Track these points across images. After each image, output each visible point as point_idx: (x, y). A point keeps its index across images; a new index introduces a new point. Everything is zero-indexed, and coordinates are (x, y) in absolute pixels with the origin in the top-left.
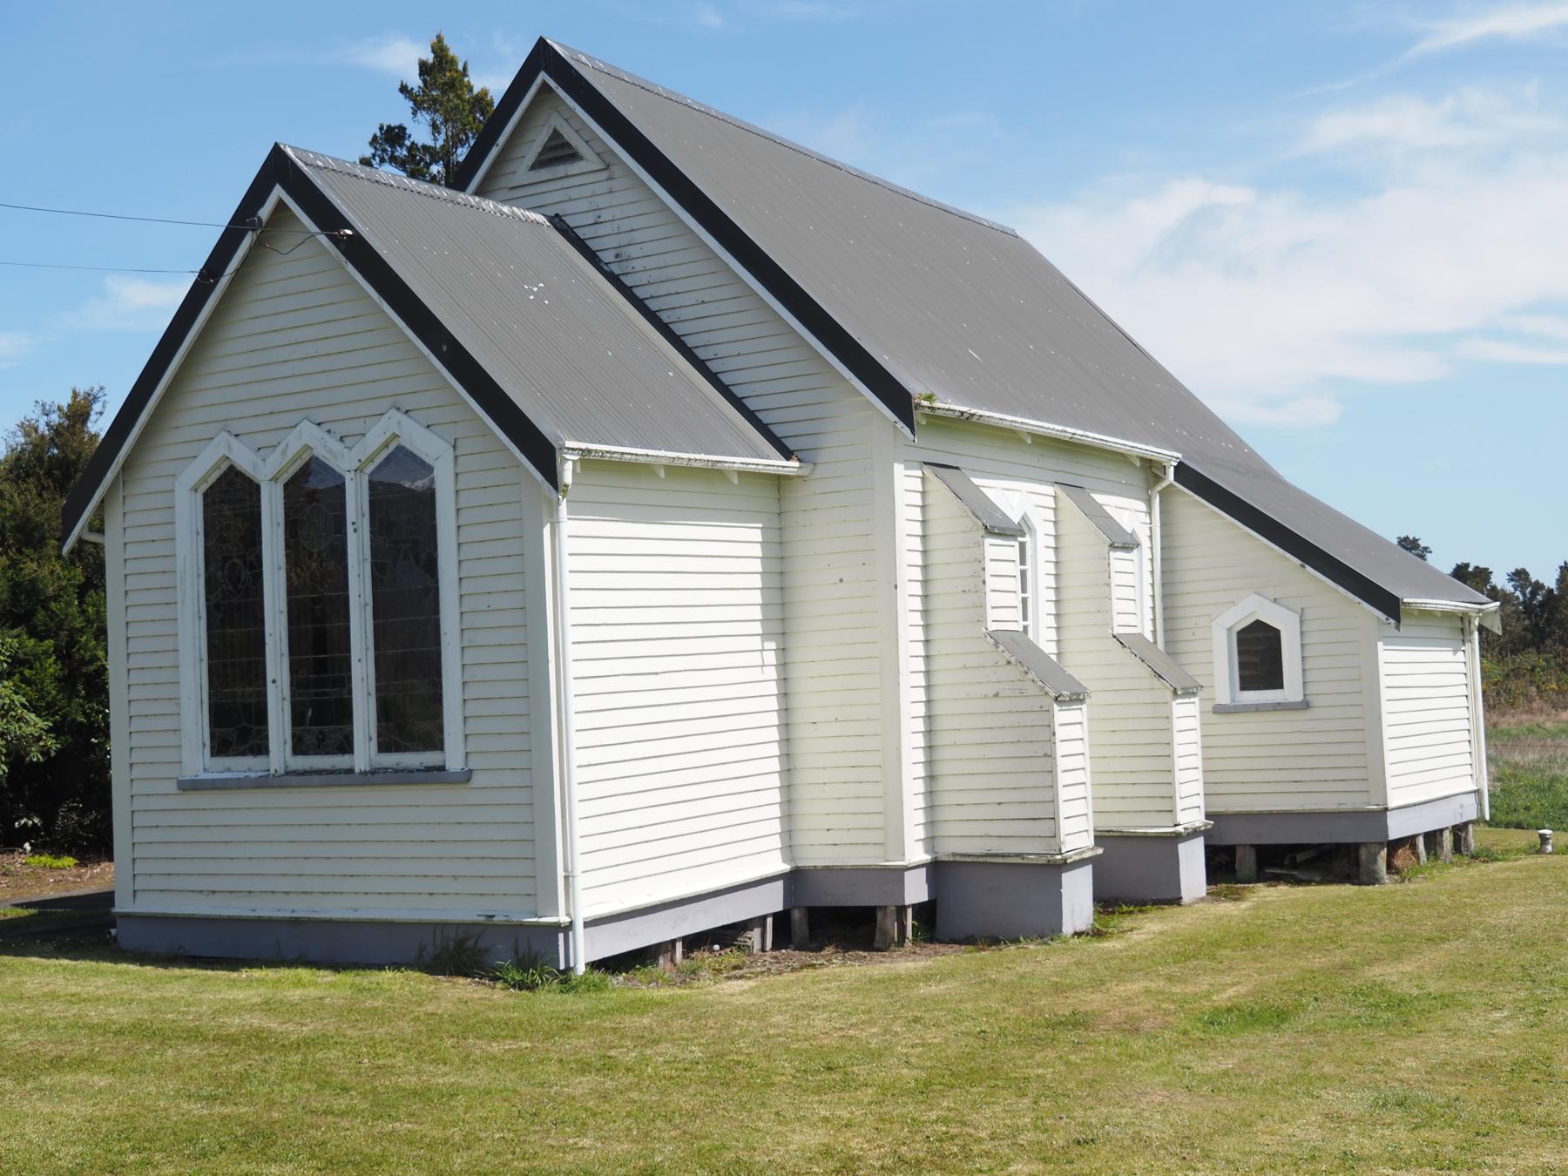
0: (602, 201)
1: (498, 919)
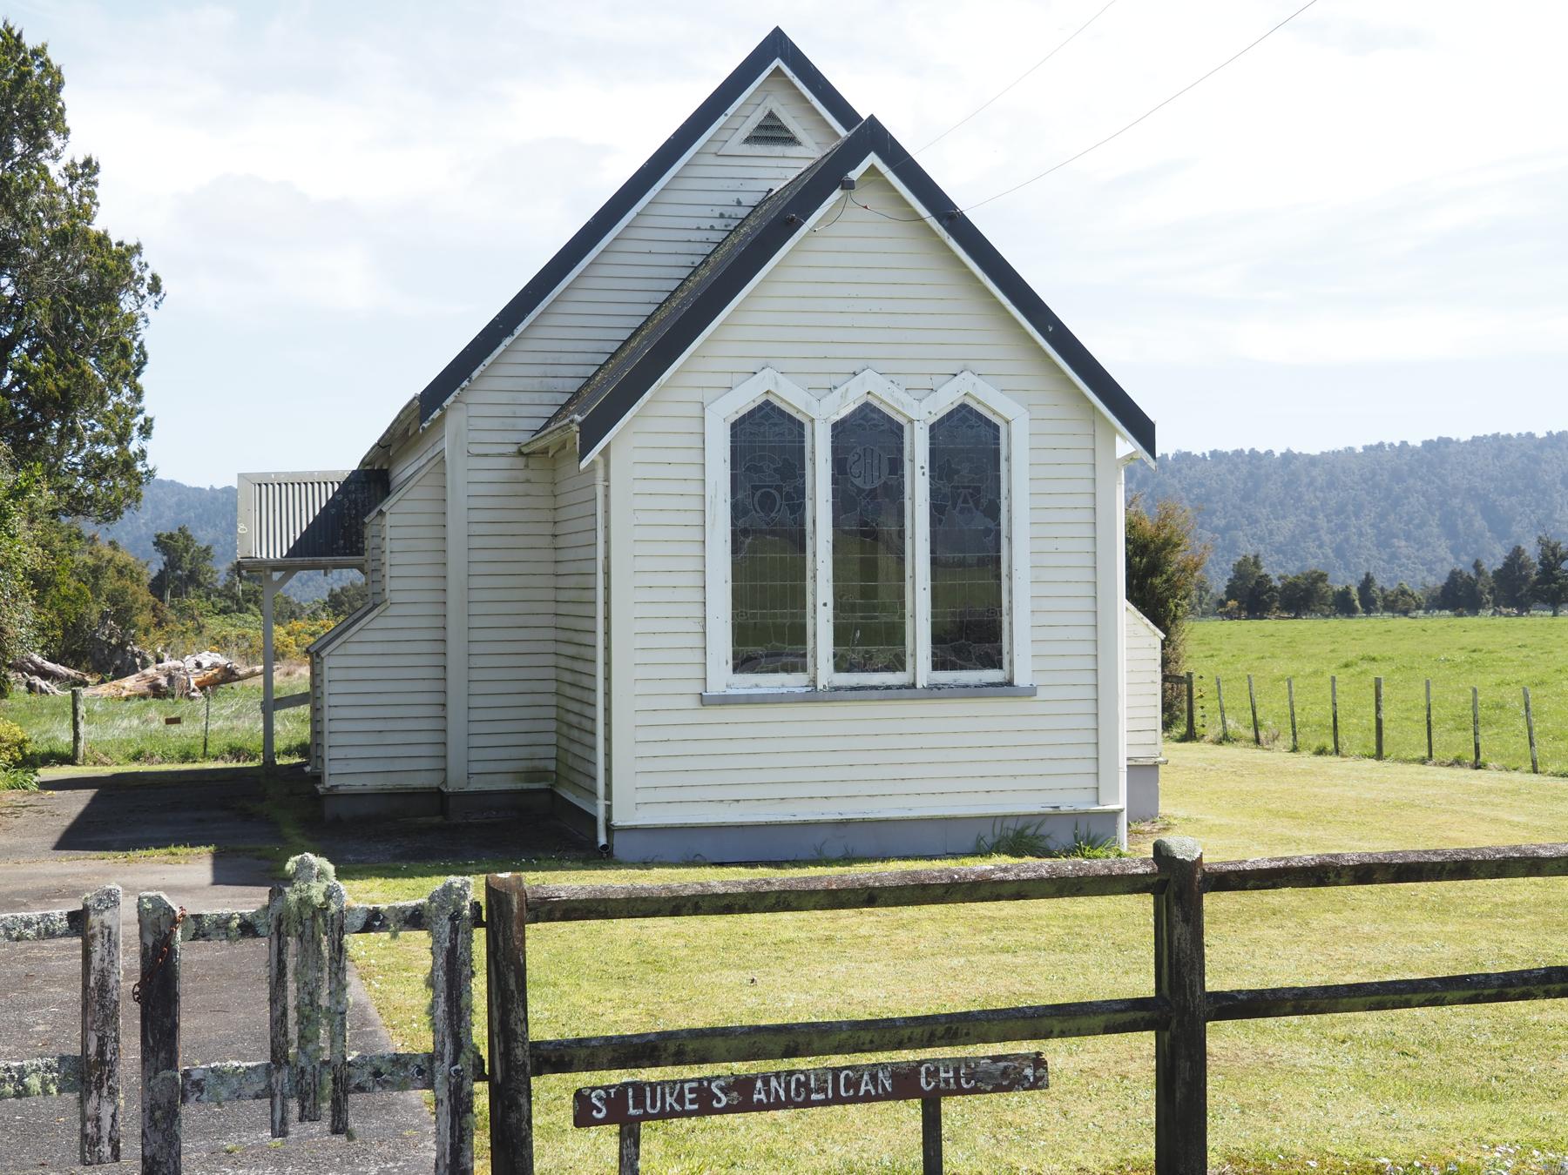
1: (1064, 809)
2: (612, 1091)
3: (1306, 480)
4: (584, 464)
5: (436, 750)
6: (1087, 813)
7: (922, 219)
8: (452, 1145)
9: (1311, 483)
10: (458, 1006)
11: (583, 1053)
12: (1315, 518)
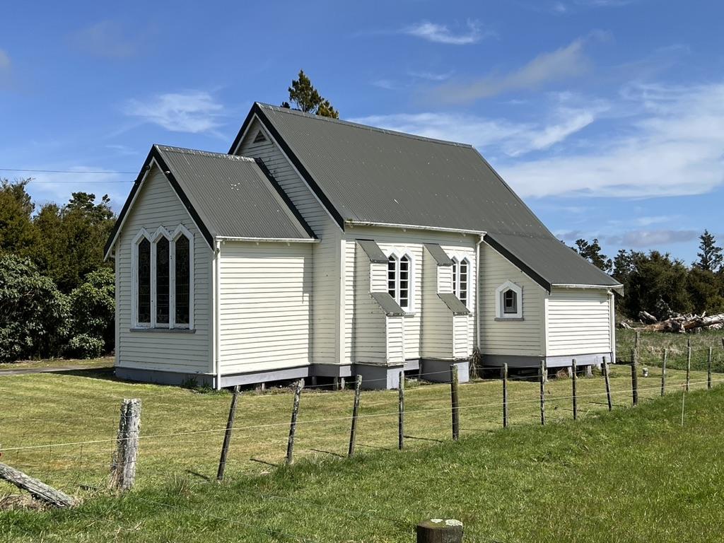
0: (271, 154)
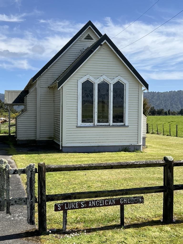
2: (62, 204)
3: (161, 96)
4: (58, 89)
5: (34, 134)
6: (136, 145)
7: (113, 51)
8: (30, 216)
9: (161, 96)
10: (32, 189)
11: (56, 197)
12: (162, 101)
